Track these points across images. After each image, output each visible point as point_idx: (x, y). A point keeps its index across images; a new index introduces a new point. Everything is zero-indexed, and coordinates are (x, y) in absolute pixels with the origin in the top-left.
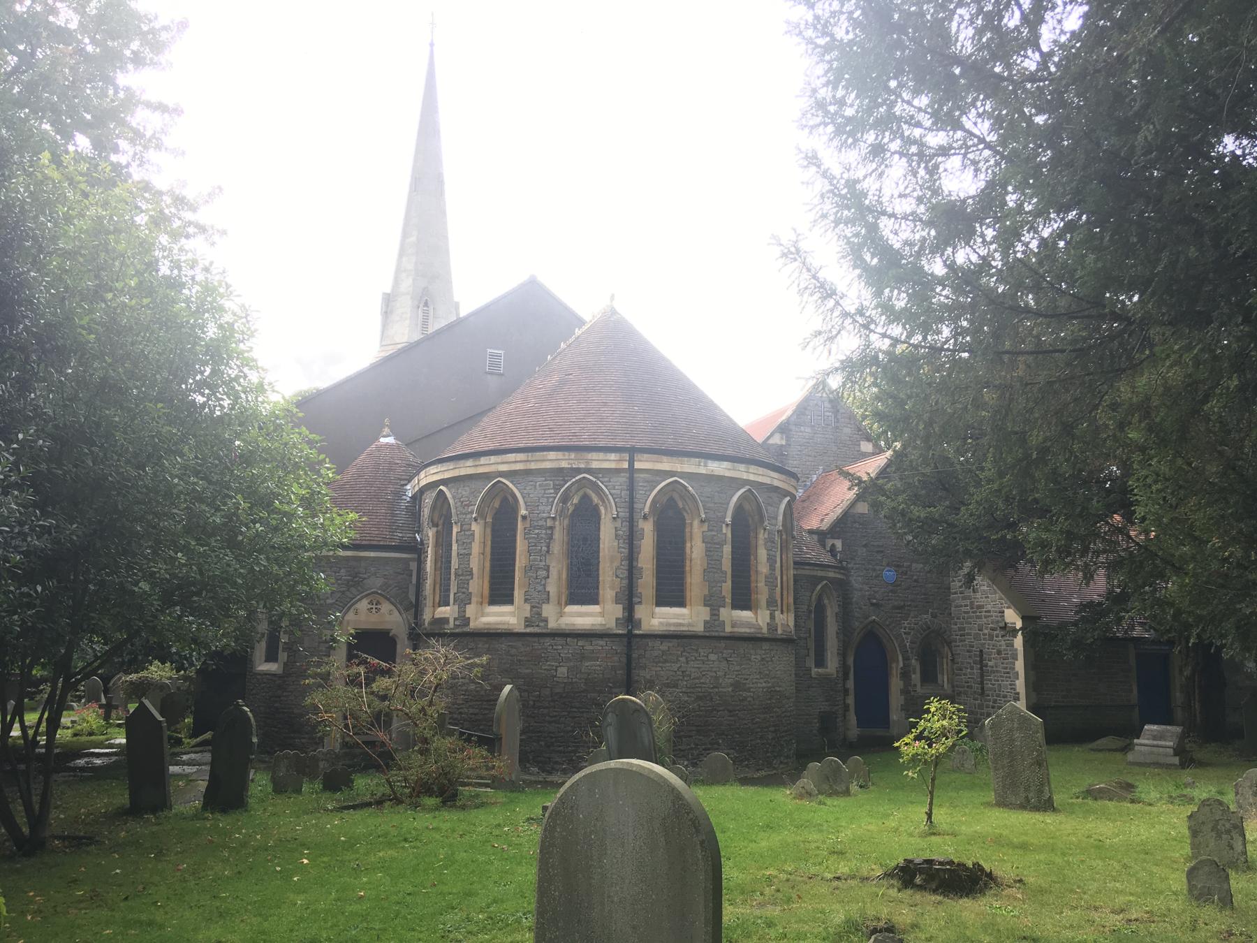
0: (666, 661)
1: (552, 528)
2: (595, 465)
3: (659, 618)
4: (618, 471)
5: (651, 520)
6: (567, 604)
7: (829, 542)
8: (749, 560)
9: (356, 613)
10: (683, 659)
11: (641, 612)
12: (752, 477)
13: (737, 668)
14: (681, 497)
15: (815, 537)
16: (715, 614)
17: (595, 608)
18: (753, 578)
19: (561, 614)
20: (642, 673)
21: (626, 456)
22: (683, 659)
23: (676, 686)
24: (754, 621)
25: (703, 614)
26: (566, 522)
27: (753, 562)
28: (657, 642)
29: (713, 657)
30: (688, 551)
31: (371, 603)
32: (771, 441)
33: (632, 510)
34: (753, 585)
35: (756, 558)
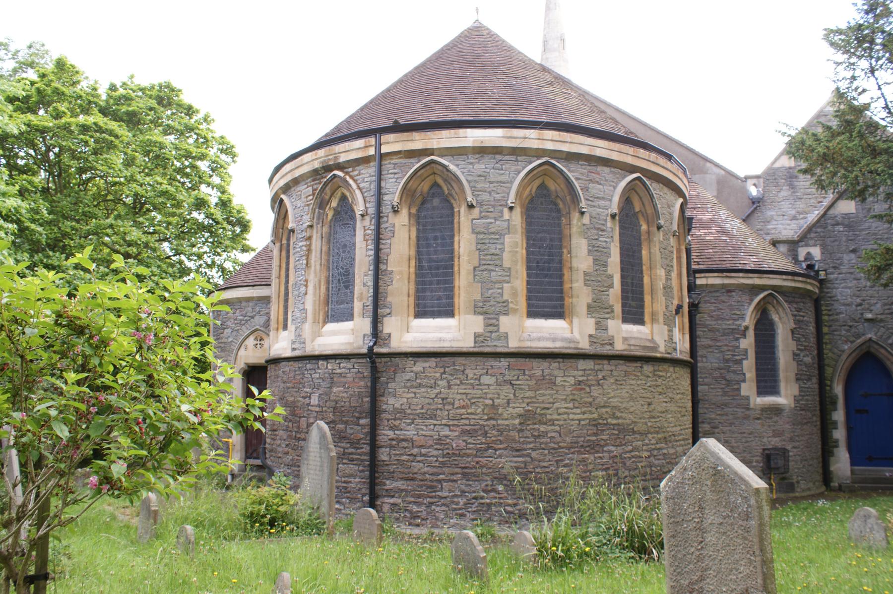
0: (420, 386)
1: (310, 238)
2: (343, 158)
3: (414, 333)
4: (366, 160)
5: (404, 212)
6: (325, 322)
7: (802, 252)
8: (561, 254)
9: (246, 349)
10: (443, 383)
11: (389, 326)
12: (549, 146)
13: (530, 394)
14: (445, 180)
15: (783, 248)
16: (492, 325)
17: (348, 325)
18: (566, 278)
19: (317, 334)
20: (391, 401)
21: (372, 140)
22: (443, 383)
23: (433, 417)
24: (567, 335)
25: (477, 324)
26: (326, 229)
27: (565, 256)
28: (410, 362)
29: (486, 380)
30: (456, 246)
31: (256, 339)
32: (777, 165)
33: (379, 204)
34: (566, 286)
35: (570, 252)
